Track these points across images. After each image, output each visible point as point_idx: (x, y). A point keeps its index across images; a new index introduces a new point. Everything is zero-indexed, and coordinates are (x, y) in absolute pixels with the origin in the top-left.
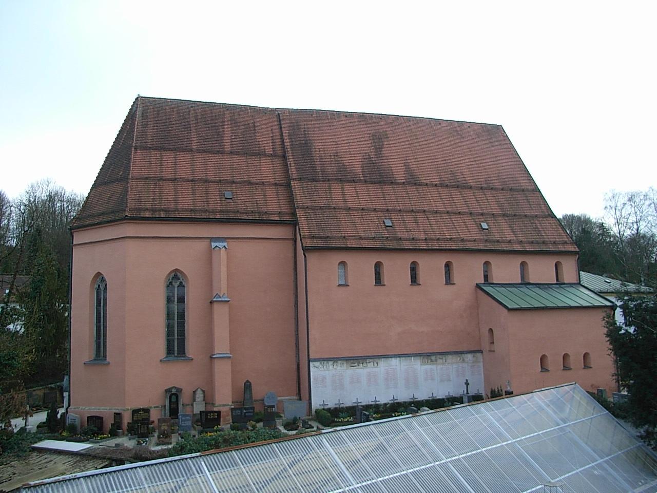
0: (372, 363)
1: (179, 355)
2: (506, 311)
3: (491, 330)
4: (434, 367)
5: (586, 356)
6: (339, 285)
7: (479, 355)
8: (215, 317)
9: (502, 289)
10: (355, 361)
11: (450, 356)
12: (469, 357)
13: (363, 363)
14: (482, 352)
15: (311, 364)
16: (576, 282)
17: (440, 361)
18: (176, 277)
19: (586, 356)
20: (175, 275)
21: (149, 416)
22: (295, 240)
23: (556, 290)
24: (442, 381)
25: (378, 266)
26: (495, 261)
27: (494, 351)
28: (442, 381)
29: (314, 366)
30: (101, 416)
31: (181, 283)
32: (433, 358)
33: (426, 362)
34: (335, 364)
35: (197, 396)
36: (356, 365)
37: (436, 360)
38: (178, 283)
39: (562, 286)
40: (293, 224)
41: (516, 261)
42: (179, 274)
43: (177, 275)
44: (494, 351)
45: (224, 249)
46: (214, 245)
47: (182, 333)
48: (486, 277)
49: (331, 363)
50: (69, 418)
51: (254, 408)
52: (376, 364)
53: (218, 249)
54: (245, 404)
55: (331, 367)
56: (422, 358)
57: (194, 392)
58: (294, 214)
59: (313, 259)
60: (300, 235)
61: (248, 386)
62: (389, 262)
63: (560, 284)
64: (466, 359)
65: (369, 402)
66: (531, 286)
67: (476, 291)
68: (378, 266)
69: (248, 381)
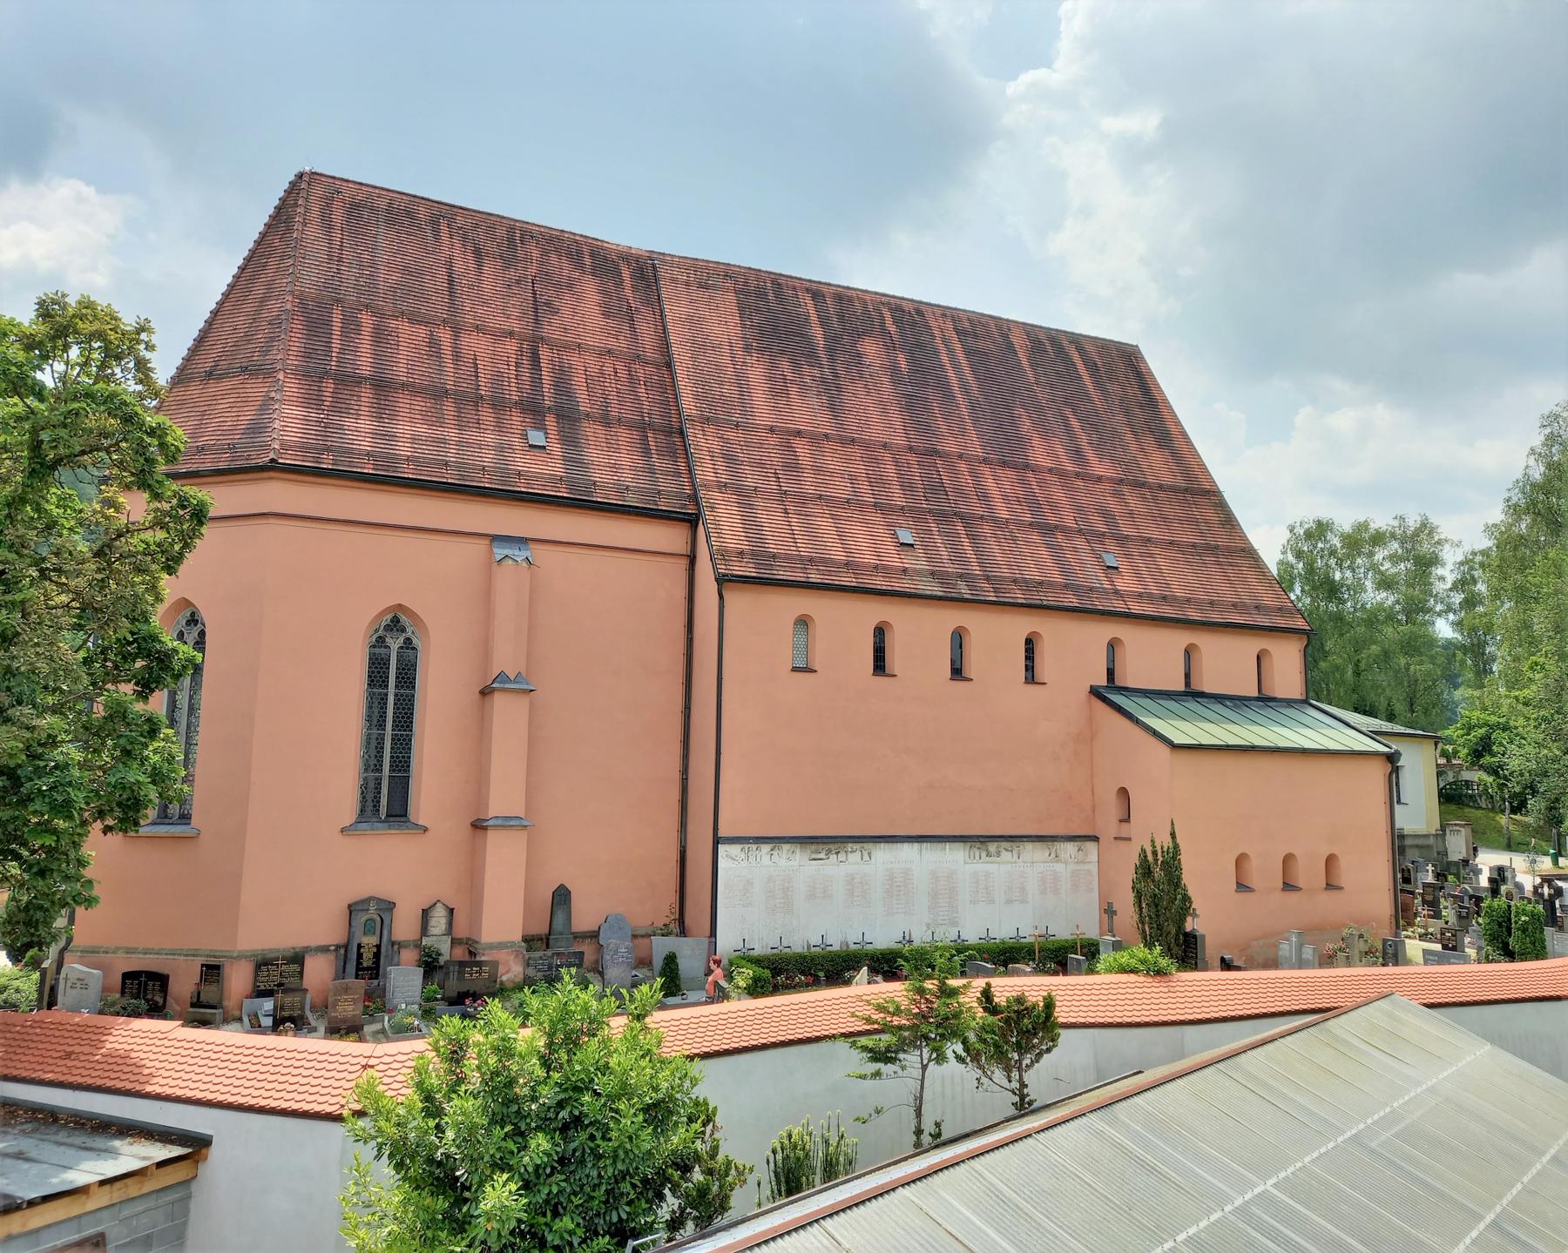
0: (858, 853)
1: (391, 819)
2: (1165, 750)
3: (1123, 793)
4: (992, 868)
5: (1330, 861)
6: (795, 669)
7: (1091, 847)
8: (855, 286)
9: (1146, 702)
10: (821, 846)
11: (1029, 846)
12: (1069, 848)
13: (837, 853)
14: (1095, 839)
15: (721, 848)
16: (1299, 697)
17: (1006, 856)
18: (395, 625)
19: (1330, 861)
20: (392, 621)
21: (301, 973)
22: (692, 559)
23: (1378, 738)
24: (1009, 902)
25: (958, 639)
26: (1128, 634)
27: (1130, 839)
28: (1009, 902)
29: (727, 856)
30: (165, 971)
31: (408, 641)
32: (992, 847)
33: (977, 857)
34: (775, 853)
35: (433, 922)
36: (822, 855)
37: (998, 854)
38: (401, 640)
39: (1270, 704)
40: (689, 521)
41: (1250, 646)
42: (403, 618)
43: (398, 621)
44: (1130, 839)
45: (524, 564)
46: (499, 552)
47: (402, 764)
48: (1111, 673)
49: (766, 848)
50: (66, 979)
51: (582, 953)
52: (866, 857)
53: (510, 562)
54: (551, 942)
55: (766, 860)
56: (969, 844)
57: (426, 914)
58: (695, 499)
59: (738, 601)
60: (710, 546)
61: (562, 897)
62: (979, 625)
63: (1265, 700)
64: (1062, 856)
65: (847, 945)
66: (1205, 700)
67: (1089, 702)
68: (958, 639)
69: (562, 887)
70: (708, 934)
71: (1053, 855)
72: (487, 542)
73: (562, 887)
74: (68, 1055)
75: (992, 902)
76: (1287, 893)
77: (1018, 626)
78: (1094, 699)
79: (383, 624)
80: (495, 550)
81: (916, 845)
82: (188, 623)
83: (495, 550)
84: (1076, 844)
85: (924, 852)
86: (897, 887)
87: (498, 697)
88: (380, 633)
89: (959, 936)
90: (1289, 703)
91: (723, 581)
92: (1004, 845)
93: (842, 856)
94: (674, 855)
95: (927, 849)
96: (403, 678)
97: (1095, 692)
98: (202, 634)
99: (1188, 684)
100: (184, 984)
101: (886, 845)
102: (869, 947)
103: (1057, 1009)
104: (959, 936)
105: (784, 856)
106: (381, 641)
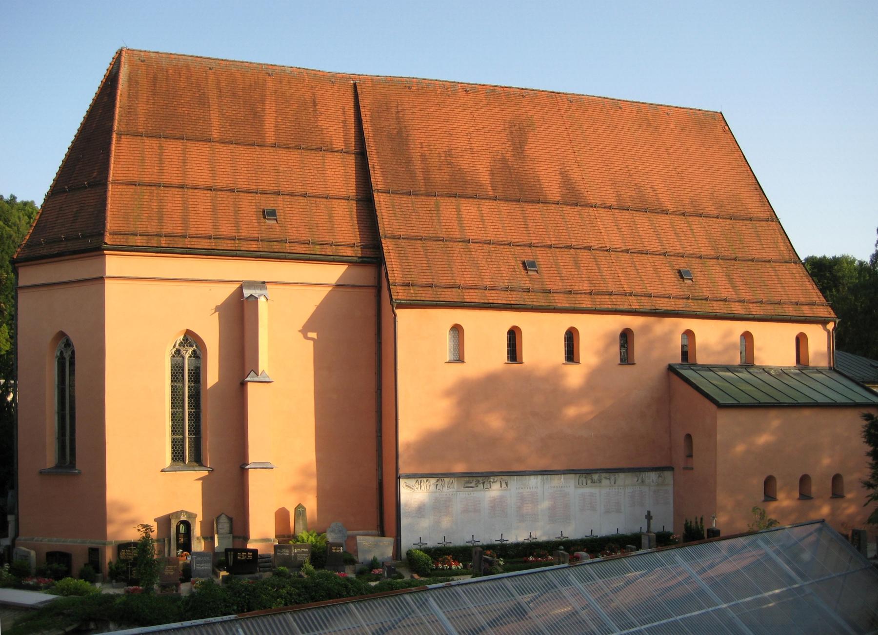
7: (668, 475)
11: (622, 476)
13: (484, 483)
14: (670, 468)
17: (605, 482)
26: (752, 327)
32: (595, 477)
33: (585, 484)
36: (472, 485)
37: (600, 481)
52: (504, 485)
56: (578, 476)
71: (640, 481)
79: (178, 342)
81: (540, 477)
82: (65, 346)
84: (657, 473)
86: (498, 506)
89: (562, 534)
90: (13, 337)
92: (604, 475)
94: (375, 485)
95: (547, 479)
96: (175, 376)
97: (671, 369)
98: (73, 352)
101: (518, 477)
102: (448, 545)
103: (280, 617)
104: (562, 534)
106: (178, 352)
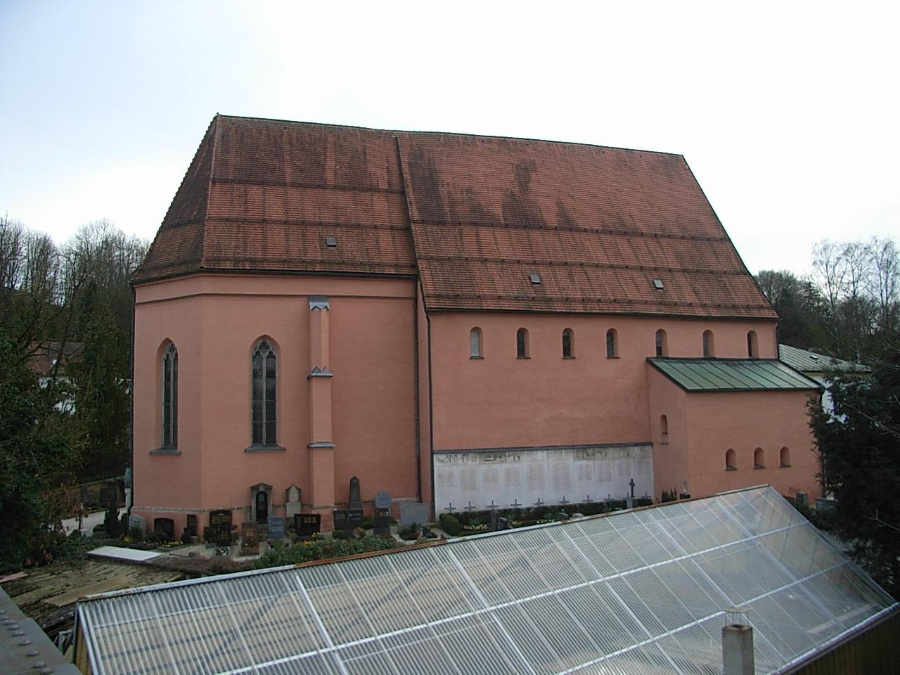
0: (512, 457)
2: (683, 393)
3: (664, 417)
7: (648, 448)
11: (611, 450)
12: (636, 450)
13: (500, 457)
15: (435, 457)
16: (774, 357)
17: (598, 455)
24: (601, 480)
25: (522, 334)
26: (667, 327)
28: (601, 480)
32: (590, 451)
34: (465, 458)
36: (492, 459)
41: (698, 330)
45: (325, 310)
46: (312, 305)
48: (659, 350)
50: (131, 520)
52: (517, 459)
53: (317, 309)
57: (288, 491)
59: (439, 324)
60: (423, 293)
61: (355, 484)
63: (753, 359)
64: (632, 454)
66: (716, 362)
68: (522, 334)
69: (355, 478)
70: (430, 501)
71: (626, 455)
72: (306, 299)
73: (355, 478)
74: (99, 581)
75: (589, 478)
76: (757, 471)
77: (602, 328)
78: (649, 366)
80: (311, 303)
83: (311, 303)
85: (550, 455)
87: (314, 380)
88: (257, 350)
91: (429, 312)
93: (503, 459)
97: (649, 361)
99: (706, 352)
100: (181, 527)
105: (470, 459)
